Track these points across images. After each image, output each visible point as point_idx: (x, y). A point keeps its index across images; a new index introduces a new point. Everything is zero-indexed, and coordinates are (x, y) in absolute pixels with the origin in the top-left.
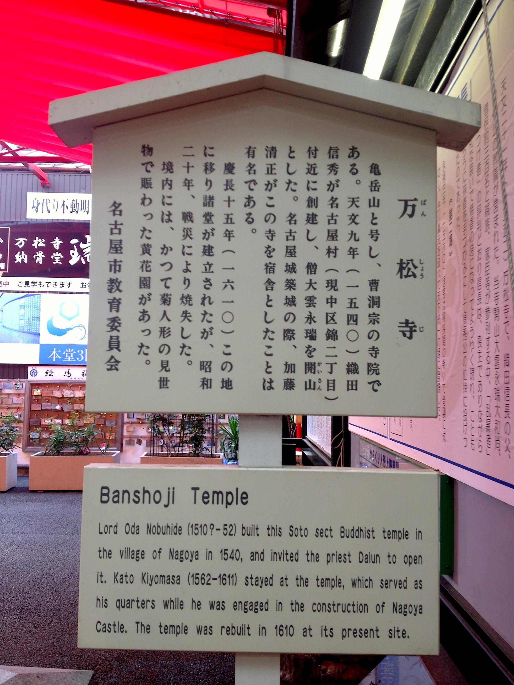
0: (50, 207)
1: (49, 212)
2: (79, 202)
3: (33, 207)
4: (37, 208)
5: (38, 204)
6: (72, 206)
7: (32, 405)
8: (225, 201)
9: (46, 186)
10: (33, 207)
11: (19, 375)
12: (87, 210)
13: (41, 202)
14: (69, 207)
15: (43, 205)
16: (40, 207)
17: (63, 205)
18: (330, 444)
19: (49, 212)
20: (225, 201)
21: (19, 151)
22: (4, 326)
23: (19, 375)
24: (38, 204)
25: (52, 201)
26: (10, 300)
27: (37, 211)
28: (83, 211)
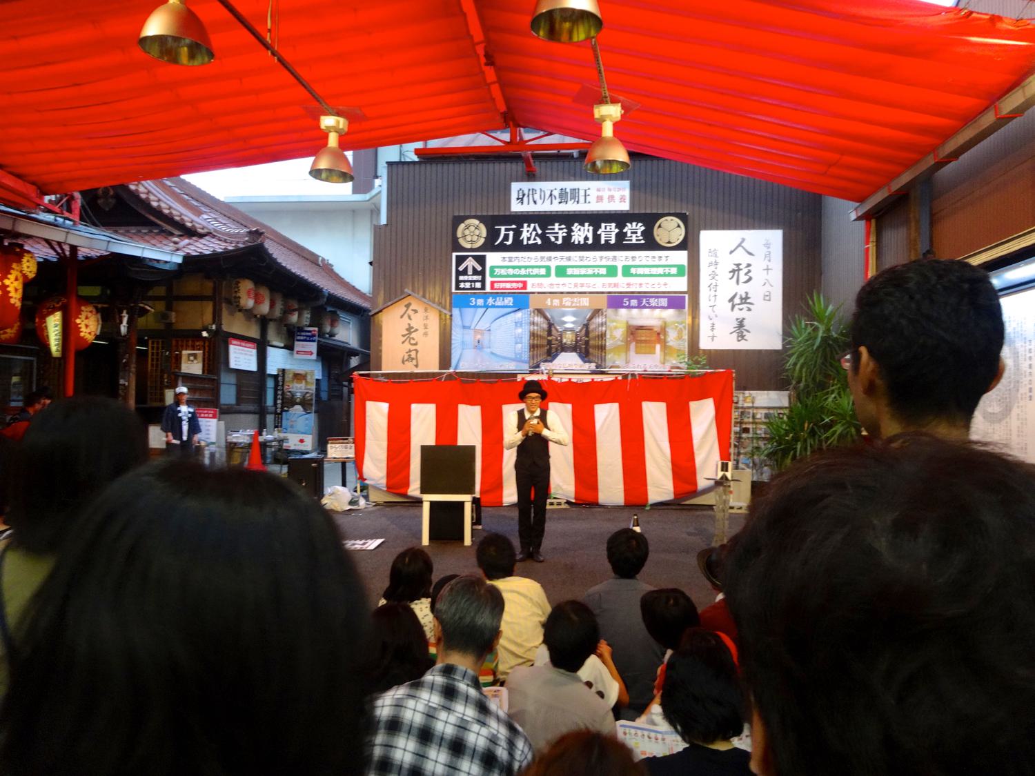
0: (537, 197)
1: (535, 202)
2: (568, 190)
3: (518, 199)
4: (522, 199)
5: (524, 195)
6: (561, 196)
7: (544, 269)
8: (768, 273)
9: (531, 176)
10: (518, 199)
11: (410, 728)
12: (577, 200)
13: (526, 192)
14: (557, 196)
15: (528, 196)
16: (525, 199)
17: (551, 195)
18: (545, 533)
19: (535, 202)
20: (768, 273)
21: (477, 326)
22: (492, 353)
23: (410, 728)
24: (524, 195)
25: (538, 192)
26: (498, 316)
27: (522, 203)
28: (573, 201)
